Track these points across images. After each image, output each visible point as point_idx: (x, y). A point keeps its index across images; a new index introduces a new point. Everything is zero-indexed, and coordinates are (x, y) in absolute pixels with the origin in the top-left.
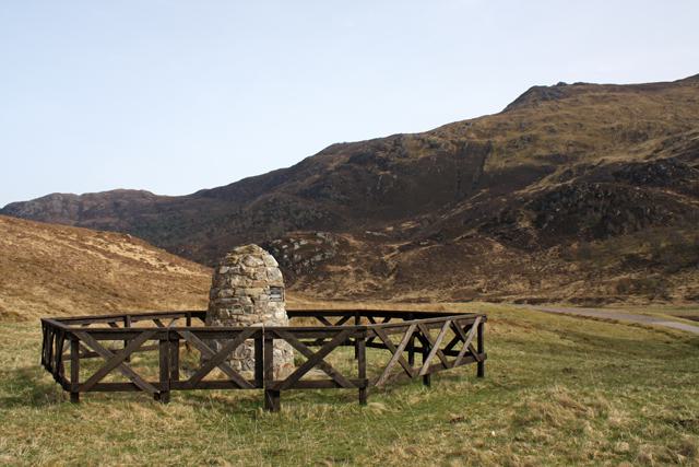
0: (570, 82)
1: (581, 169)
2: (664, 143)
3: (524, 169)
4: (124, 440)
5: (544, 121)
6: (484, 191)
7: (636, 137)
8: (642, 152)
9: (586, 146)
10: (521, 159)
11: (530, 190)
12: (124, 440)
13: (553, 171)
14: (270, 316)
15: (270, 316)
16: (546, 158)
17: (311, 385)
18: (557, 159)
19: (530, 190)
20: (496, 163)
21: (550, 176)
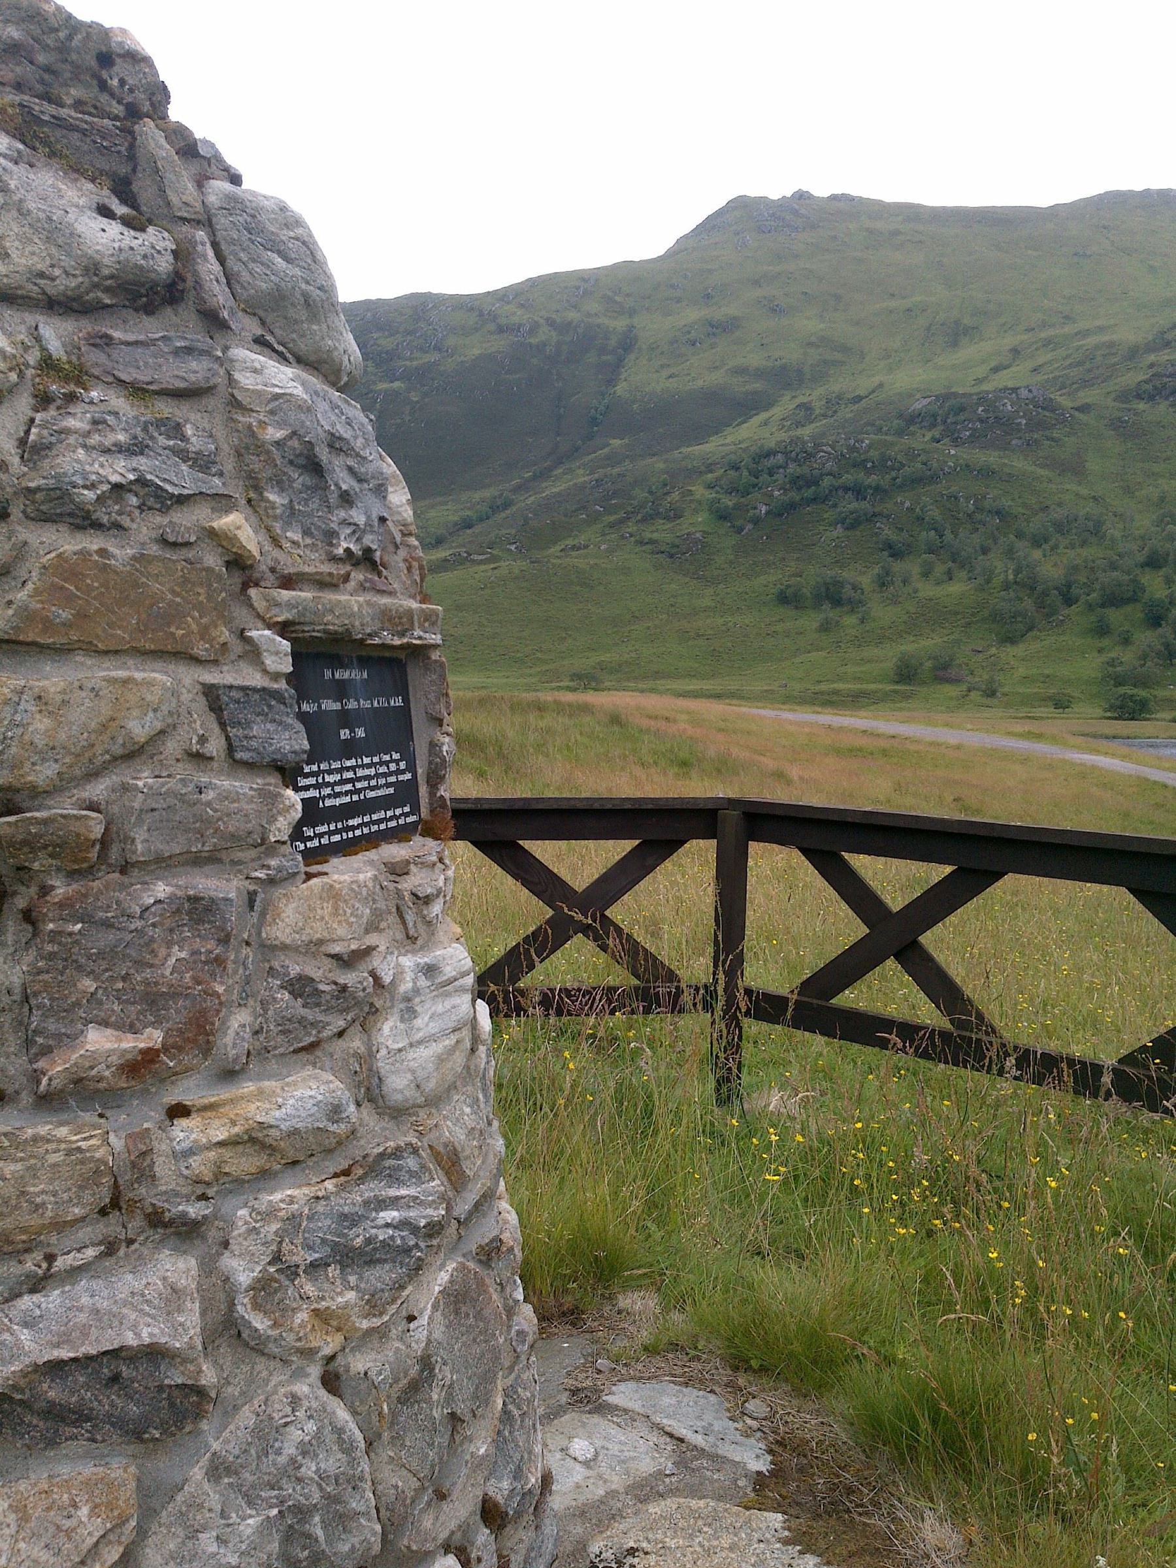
0: (821, 190)
1: (834, 403)
2: (1015, 351)
3: (711, 397)
4: (1135, 829)
5: (757, 283)
6: (616, 442)
7: (957, 334)
8: (964, 369)
9: (845, 349)
10: (702, 372)
11: (714, 447)
12: (1135, 829)
13: (769, 405)
14: (297, 1097)
15: (297, 1097)
16: (760, 374)
17: (864, 1029)
18: (785, 378)
19: (714, 447)
20: (642, 379)
21: (763, 416)
